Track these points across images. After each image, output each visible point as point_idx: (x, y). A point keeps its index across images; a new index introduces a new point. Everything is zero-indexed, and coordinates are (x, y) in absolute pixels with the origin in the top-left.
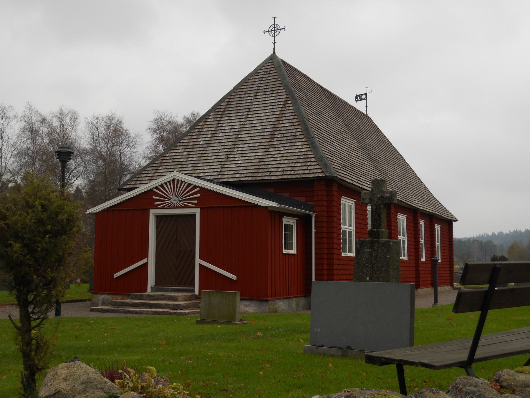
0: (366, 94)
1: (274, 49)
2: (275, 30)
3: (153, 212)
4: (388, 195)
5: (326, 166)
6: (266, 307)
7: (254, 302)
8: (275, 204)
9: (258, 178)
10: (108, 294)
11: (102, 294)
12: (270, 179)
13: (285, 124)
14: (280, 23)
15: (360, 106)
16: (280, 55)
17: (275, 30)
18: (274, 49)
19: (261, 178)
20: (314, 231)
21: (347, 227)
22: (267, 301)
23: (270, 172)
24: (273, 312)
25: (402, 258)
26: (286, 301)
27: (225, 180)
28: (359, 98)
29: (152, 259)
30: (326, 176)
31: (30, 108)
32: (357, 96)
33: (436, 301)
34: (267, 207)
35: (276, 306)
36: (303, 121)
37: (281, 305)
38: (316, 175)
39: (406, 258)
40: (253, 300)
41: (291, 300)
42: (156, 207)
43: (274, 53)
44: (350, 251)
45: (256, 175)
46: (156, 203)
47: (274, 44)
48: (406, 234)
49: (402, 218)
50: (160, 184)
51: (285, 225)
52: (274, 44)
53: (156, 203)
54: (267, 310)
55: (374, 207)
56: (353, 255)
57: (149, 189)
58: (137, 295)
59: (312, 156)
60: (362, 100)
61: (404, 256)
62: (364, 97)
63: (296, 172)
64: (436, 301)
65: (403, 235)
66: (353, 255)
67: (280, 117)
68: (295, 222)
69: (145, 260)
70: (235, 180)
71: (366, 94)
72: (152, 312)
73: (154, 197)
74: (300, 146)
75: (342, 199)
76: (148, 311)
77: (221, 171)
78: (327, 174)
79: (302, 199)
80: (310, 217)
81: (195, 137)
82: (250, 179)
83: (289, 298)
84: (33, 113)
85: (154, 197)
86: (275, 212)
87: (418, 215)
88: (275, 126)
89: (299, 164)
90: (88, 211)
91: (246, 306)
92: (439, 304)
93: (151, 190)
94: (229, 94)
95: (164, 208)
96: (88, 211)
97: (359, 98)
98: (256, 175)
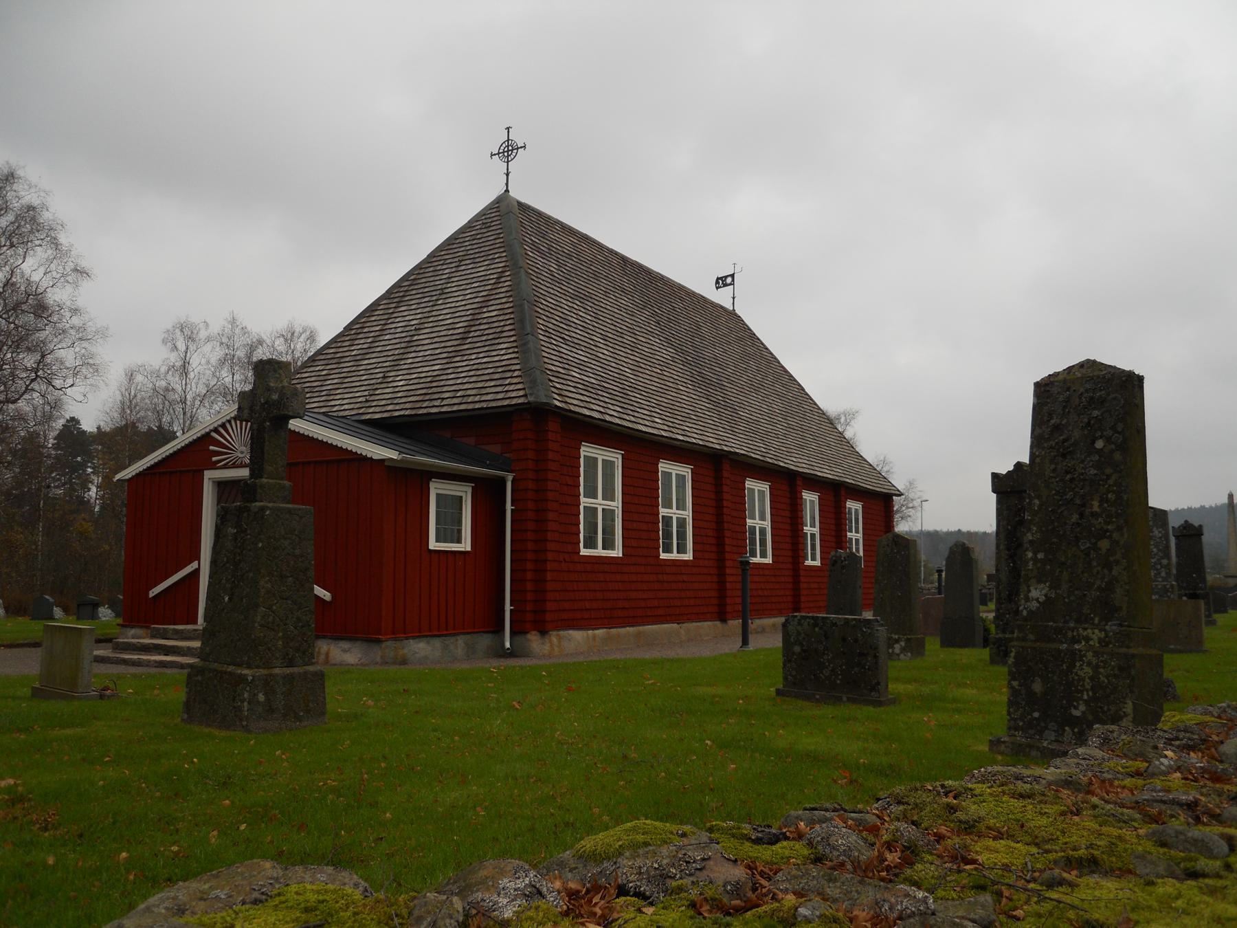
0: (732, 276)
1: (507, 184)
2: (508, 151)
3: (209, 475)
4: (275, 397)
5: (534, 383)
6: (377, 653)
7: (358, 644)
8: (394, 455)
9: (421, 412)
10: (141, 627)
11: (132, 627)
12: (440, 413)
13: (491, 313)
14: (517, 139)
15: (722, 298)
16: (517, 194)
17: (508, 151)
18: (507, 184)
19: (425, 411)
20: (509, 507)
21: (757, 521)
22: (379, 641)
23: (443, 399)
24: (394, 663)
25: (809, 562)
26: (437, 643)
27: (368, 417)
28: (721, 282)
29: (205, 563)
30: (529, 403)
31: (233, 322)
32: (717, 282)
33: (745, 642)
34: (383, 460)
35: (405, 651)
36: (521, 306)
37: (420, 648)
38: (514, 402)
39: (817, 563)
40: (356, 639)
41: (452, 639)
42: (213, 466)
43: (507, 191)
44: (763, 555)
45: (418, 405)
46: (214, 459)
47: (507, 175)
48: (768, 516)
49: (810, 498)
50: (220, 423)
51: (438, 495)
52: (507, 175)
53: (214, 459)
54: (378, 659)
55: (255, 426)
56: (769, 560)
57: (203, 432)
58: (159, 629)
59: (518, 367)
60: (725, 285)
61: (813, 559)
62: (729, 280)
63: (484, 398)
64: (745, 642)
65: (857, 532)
66: (769, 560)
67: (485, 303)
68: (470, 490)
69: (195, 565)
70: (385, 415)
71: (732, 276)
72: (156, 661)
73: (211, 448)
74: (504, 352)
75: (583, 448)
76: (149, 661)
77: (367, 401)
78: (531, 399)
79: (496, 449)
80: (503, 482)
81: (347, 343)
82: (407, 413)
83: (446, 635)
84: (237, 331)
85: (211, 448)
86: (395, 468)
87: (799, 483)
88: (474, 320)
89: (493, 383)
90: (118, 477)
91: (345, 651)
92: (751, 647)
93: (208, 434)
94: (419, 267)
95: (225, 467)
96: (118, 477)
97: (721, 282)
98: (418, 405)
